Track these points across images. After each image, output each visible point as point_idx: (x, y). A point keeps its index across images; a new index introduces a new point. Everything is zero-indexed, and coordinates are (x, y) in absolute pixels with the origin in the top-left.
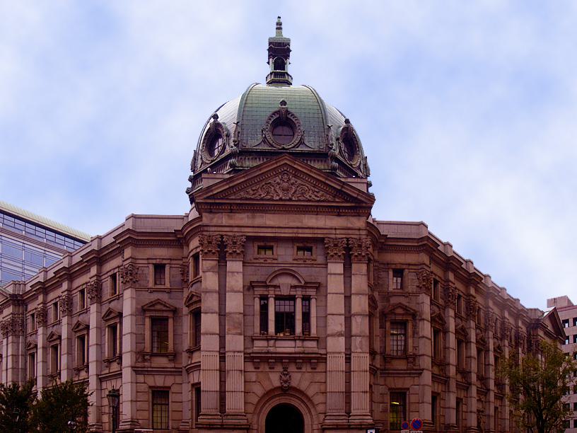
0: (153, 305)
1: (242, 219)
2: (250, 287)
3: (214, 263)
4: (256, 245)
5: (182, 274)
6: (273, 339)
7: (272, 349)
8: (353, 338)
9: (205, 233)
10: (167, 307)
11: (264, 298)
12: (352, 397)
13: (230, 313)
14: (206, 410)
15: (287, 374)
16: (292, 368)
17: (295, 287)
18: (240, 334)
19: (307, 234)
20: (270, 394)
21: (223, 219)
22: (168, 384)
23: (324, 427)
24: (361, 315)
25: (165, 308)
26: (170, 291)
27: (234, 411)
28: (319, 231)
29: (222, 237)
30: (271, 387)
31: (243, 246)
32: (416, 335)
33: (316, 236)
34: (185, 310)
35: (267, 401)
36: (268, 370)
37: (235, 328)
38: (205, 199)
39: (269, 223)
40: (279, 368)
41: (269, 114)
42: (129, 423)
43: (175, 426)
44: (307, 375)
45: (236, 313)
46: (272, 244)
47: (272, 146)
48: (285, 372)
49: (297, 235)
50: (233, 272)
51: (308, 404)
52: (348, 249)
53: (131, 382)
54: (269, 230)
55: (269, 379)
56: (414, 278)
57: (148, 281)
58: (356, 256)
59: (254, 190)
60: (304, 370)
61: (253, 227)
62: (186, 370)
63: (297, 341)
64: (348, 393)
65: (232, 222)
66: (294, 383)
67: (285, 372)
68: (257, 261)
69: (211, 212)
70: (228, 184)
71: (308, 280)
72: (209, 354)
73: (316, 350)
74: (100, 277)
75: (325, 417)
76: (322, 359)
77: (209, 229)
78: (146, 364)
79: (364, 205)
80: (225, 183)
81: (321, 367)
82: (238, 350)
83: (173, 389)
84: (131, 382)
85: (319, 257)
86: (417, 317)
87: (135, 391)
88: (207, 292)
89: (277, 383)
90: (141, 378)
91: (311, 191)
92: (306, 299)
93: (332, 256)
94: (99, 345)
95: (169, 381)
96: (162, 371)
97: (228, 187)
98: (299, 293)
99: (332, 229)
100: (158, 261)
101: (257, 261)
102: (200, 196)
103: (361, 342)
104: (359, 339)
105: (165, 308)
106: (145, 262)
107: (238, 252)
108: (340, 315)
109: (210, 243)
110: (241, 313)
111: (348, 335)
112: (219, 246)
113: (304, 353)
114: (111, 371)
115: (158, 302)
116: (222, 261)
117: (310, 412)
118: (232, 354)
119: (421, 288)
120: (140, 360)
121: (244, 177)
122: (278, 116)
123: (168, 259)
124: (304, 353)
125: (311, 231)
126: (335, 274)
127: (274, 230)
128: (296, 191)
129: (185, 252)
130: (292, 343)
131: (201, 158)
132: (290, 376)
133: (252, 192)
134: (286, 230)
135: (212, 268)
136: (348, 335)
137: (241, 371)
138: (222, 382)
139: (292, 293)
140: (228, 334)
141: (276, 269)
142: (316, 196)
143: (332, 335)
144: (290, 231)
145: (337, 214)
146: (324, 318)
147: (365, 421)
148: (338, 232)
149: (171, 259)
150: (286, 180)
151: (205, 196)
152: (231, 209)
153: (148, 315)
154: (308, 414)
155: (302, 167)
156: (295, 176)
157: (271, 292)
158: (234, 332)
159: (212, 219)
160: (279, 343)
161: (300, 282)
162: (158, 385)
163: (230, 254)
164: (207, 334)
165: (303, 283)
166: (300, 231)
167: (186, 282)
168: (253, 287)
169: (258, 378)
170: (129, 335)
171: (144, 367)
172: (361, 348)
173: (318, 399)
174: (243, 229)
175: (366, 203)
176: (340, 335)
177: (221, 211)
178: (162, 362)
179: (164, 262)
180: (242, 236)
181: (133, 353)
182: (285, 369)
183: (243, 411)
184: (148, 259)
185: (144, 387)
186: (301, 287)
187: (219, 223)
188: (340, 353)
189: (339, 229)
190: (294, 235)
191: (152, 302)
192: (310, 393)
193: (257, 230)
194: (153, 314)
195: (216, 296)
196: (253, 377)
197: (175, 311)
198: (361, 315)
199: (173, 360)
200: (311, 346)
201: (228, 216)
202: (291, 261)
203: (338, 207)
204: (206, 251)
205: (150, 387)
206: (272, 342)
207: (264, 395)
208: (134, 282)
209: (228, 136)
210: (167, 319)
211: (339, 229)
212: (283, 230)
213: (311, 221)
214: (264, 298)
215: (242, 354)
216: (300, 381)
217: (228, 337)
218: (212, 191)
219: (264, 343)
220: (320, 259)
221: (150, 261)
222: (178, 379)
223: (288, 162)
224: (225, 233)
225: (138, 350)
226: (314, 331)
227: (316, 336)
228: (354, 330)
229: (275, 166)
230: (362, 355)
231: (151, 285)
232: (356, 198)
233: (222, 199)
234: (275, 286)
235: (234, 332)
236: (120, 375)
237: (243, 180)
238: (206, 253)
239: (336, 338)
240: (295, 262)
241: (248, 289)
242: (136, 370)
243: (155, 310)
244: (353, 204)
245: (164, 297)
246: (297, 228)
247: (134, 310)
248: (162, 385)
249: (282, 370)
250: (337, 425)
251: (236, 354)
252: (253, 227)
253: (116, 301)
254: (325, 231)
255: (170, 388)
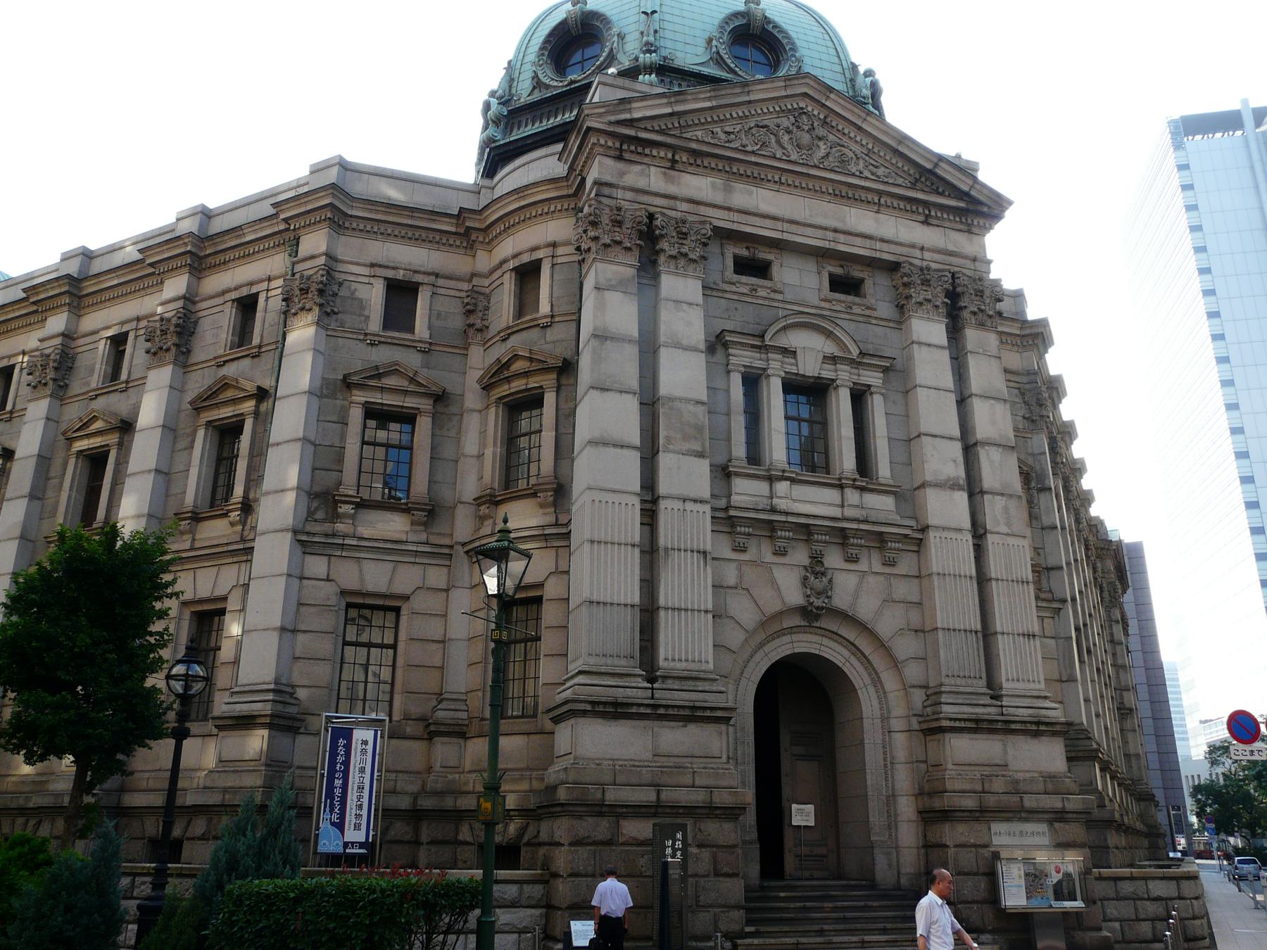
0: (379, 376)
1: (698, 185)
2: (717, 344)
3: (631, 272)
4: (732, 250)
5: (469, 313)
6: (787, 479)
7: (782, 504)
8: (986, 497)
9: (604, 200)
10: (420, 385)
11: (752, 382)
12: (1001, 646)
13: (671, 399)
14: (602, 661)
15: (823, 574)
16: (833, 559)
17: (832, 359)
18: (701, 455)
19: (858, 248)
20: (771, 625)
21: (653, 178)
22: (400, 587)
23: (432, 728)
24: (999, 445)
25: (412, 388)
26: (427, 350)
27: (684, 665)
28: (885, 247)
29: (651, 217)
30: (778, 607)
31: (705, 245)
32: (1034, 522)
33: (878, 255)
34: (472, 399)
35: (761, 645)
36: (769, 557)
37: (686, 438)
38: (611, 123)
39: (764, 208)
40: (800, 556)
41: (728, 12)
42: (270, 696)
43: (415, 710)
44: (871, 579)
45: (688, 401)
46: (770, 257)
47: (735, 73)
48: (816, 567)
49: (832, 246)
50: (676, 301)
51: (878, 661)
52: (953, 296)
53: (289, 575)
54: (768, 223)
55: (773, 583)
56: (1018, 400)
57: (368, 317)
58: (974, 313)
59: (728, 133)
60: (863, 566)
61: (729, 209)
62: (467, 552)
63: (848, 491)
64: (987, 634)
65: (672, 189)
66: (840, 600)
67: (816, 567)
68: (733, 288)
69: (620, 158)
70: (670, 104)
71: (870, 348)
72: (610, 497)
73: (896, 518)
74: (194, 303)
75: (440, 703)
76: (917, 540)
77: (614, 192)
78: (340, 527)
79: (985, 209)
80: (665, 101)
81: (906, 564)
82: (692, 495)
83: (418, 602)
84: (289, 575)
85: (880, 303)
86: (1033, 484)
87: (294, 601)
88: (606, 338)
89: (795, 597)
90: (317, 565)
91: (861, 162)
92: (859, 397)
93: (921, 304)
94: (165, 474)
95: (406, 579)
96: (389, 549)
97: (669, 110)
98: (845, 375)
99: (913, 246)
100: (400, 275)
101: (733, 288)
102: (600, 115)
103: (1006, 509)
104: (1000, 502)
105: (412, 388)
106: (365, 271)
107: (692, 256)
108: (951, 439)
109: (618, 223)
110: (703, 403)
111: (974, 489)
112: (641, 235)
113: (865, 521)
114: (197, 545)
115: (394, 370)
116: (649, 267)
117: (877, 681)
118: (678, 505)
119: (1033, 421)
120: (320, 515)
121: (709, 99)
122: (744, 21)
123: (429, 274)
124: (865, 521)
125: (868, 243)
126: (929, 345)
127: (779, 225)
128: (828, 155)
129: (483, 261)
130: (832, 495)
131: (536, 76)
132: (830, 581)
133: (723, 136)
134: (809, 231)
135: (621, 282)
136: (974, 489)
137: (705, 553)
138: (649, 584)
139: (825, 374)
140: (667, 450)
141: (781, 313)
142: (873, 174)
143: (937, 485)
144: (819, 233)
145: (922, 218)
146: (908, 441)
147: (1044, 712)
148: (927, 255)
149: (437, 275)
150: (806, 128)
151: (613, 118)
152: (674, 161)
153: (363, 399)
154: (872, 690)
155: (843, 107)
156: (824, 123)
157: (777, 368)
158: (686, 446)
159: (622, 174)
160: (800, 491)
161: (850, 352)
162: (371, 587)
163: (671, 257)
164: (606, 444)
165: (855, 352)
166: (842, 238)
167: (480, 330)
168: (726, 345)
169: (741, 576)
170: (299, 445)
171: (334, 535)
172: (1008, 524)
173: (905, 647)
174: (703, 210)
175: (989, 207)
176: (953, 486)
177: (646, 160)
178: (393, 525)
179: (418, 278)
180: (703, 222)
181: (303, 493)
182: (817, 559)
183: (711, 666)
184: (372, 265)
185: (326, 592)
186: (852, 362)
187: (641, 183)
188: (960, 530)
189: (929, 250)
190: (826, 245)
191: (377, 367)
192: (885, 628)
193: (736, 217)
194: (377, 398)
195: (632, 352)
196: (731, 576)
197: (440, 398)
198: (999, 445)
199: (425, 524)
200: (881, 505)
201: (665, 174)
202: (816, 302)
203: (926, 204)
204: (608, 241)
205: (344, 593)
206: (782, 487)
207: (763, 625)
208: (328, 314)
209: (621, 37)
210: (408, 418)
211: (929, 250)
212: (800, 230)
213: (861, 219)
214: (752, 382)
215: (707, 508)
216: (856, 595)
217: (666, 461)
218: (630, 111)
219: (762, 488)
220: (885, 309)
221: (379, 272)
222: (437, 576)
223: (810, 92)
224: (659, 210)
225: (317, 489)
226: (884, 470)
227: (891, 482)
228: (989, 478)
229: (783, 93)
230: (1011, 540)
231: (375, 325)
232: (967, 194)
233: (653, 131)
234: (785, 351)
235: (686, 446)
236: (245, 552)
237: (708, 104)
238: (606, 246)
239: (948, 493)
240: (823, 304)
241: (711, 349)
242: (304, 542)
243: (382, 389)
244: (962, 204)
245: (412, 360)
246: (835, 231)
247: (318, 383)
248: (383, 589)
249: (806, 562)
250: (977, 721)
251: (690, 506)
252: (729, 209)
253: (247, 362)
254: (899, 250)
255: (406, 598)
